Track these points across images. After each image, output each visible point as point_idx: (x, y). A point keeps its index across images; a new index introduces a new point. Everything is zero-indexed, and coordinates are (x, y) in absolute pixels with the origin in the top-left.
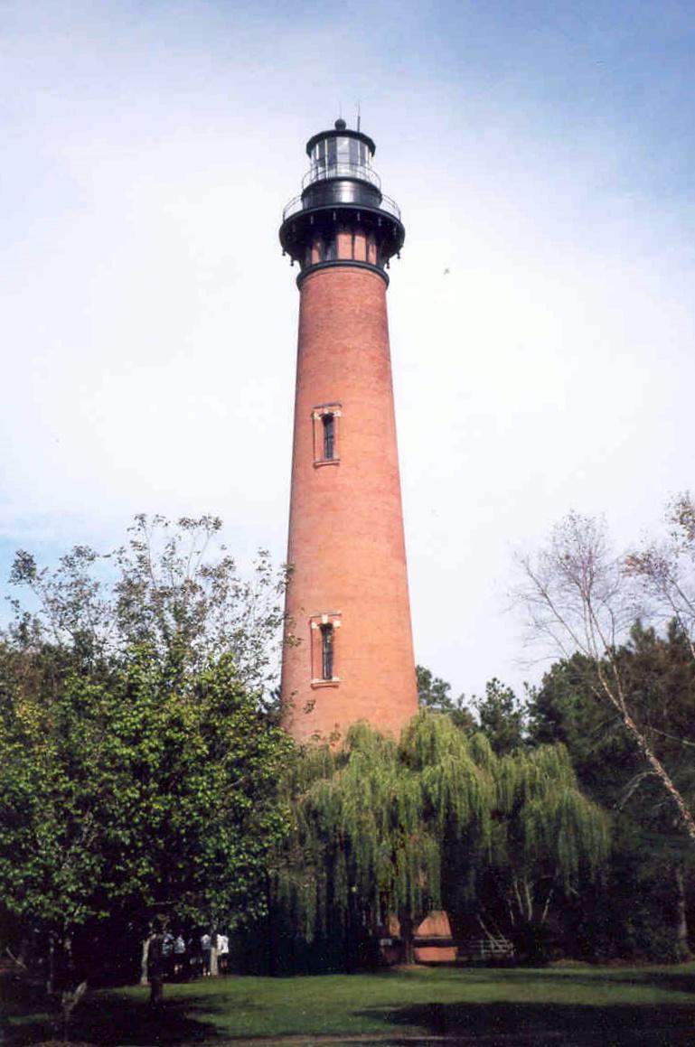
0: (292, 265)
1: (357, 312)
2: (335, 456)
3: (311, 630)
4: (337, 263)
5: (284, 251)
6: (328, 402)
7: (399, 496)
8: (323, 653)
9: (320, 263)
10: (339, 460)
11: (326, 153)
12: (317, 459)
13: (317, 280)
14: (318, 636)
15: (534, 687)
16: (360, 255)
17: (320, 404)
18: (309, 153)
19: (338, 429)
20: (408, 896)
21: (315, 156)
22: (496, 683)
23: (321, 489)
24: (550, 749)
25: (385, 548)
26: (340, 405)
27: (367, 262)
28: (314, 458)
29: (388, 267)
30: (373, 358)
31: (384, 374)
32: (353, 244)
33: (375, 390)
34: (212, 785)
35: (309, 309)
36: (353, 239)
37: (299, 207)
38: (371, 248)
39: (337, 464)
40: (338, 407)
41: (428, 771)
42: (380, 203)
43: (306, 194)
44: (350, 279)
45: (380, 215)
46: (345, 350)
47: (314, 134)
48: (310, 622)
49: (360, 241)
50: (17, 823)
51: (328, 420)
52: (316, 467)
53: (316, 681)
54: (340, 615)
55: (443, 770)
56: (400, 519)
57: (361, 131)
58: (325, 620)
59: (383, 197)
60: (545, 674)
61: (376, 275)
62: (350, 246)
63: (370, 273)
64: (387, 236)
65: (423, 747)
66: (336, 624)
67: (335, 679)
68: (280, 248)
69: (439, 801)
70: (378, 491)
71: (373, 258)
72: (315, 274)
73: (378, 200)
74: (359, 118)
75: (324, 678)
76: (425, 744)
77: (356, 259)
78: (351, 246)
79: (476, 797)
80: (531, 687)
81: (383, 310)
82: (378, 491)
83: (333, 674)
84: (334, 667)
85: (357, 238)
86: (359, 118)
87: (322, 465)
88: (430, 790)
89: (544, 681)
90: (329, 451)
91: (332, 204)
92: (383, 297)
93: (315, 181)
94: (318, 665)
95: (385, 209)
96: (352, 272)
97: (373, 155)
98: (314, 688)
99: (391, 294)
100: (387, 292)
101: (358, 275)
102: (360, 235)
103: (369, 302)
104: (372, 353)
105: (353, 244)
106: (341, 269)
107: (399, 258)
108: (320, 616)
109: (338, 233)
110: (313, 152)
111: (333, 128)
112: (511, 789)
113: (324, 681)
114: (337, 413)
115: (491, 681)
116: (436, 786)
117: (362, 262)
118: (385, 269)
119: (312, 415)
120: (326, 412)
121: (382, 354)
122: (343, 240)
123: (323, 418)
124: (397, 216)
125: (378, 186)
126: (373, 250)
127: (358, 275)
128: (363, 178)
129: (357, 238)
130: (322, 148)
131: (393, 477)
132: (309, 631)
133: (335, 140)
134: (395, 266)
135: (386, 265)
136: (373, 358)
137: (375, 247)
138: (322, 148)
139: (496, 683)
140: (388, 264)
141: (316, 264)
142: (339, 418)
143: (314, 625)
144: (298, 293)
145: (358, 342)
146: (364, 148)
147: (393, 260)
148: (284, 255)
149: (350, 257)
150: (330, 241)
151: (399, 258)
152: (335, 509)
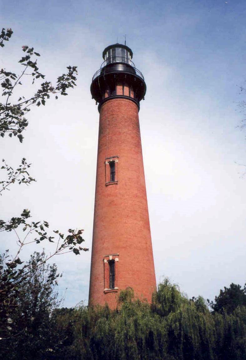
1: (126, 117)
2: (116, 180)
3: (104, 263)
4: (116, 97)
6: (112, 156)
7: (146, 200)
8: (110, 276)
9: (108, 97)
10: (117, 182)
11: (111, 54)
12: (107, 182)
13: (106, 105)
14: (108, 266)
15: (212, 302)
17: (109, 157)
19: (117, 169)
22: (194, 299)
23: (109, 195)
25: (141, 223)
26: (118, 157)
27: (129, 97)
28: (106, 182)
32: (123, 90)
33: (134, 151)
36: (123, 88)
38: (131, 92)
39: (117, 184)
40: (117, 158)
41: (171, 316)
43: (103, 70)
45: (135, 77)
46: (120, 133)
47: (106, 47)
48: (104, 260)
49: (126, 89)
51: (112, 164)
52: (107, 186)
53: (106, 289)
54: (118, 255)
55: (181, 313)
56: (149, 219)
57: (126, 45)
58: (111, 258)
60: (216, 297)
61: (134, 103)
62: (122, 91)
64: (139, 89)
65: (167, 302)
66: (117, 259)
67: (116, 288)
69: (179, 335)
70: (136, 196)
74: (125, 41)
75: (110, 288)
76: (168, 299)
78: (122, 90)
79: (204, 331)
80: (210, 302)
81: (137, 118)
82: (136, 196)
83: (115, 285)
84: (115, 282)
85: (125, 87)
86: (125, 41)
87: (109, 185)
88: (173, 326)
89: (216, 300)
90: (113, 178)
91: (115, 71)
92: (138, 114)
94: (107, 284)
98: (105, 293)
102: (125, 86)
103: (130, 113)
104: (132, 135)
105: (123, 90)
106: (118, 99)
108: (109, 256)
110: (105, 56)
112: (222, 332)
113: (110, 289)
114: (117, 161)
115: (192, 299)
116: (177, 324)
117: (128, 97)
119: (105, 163)
120: (111, 160)
121: (137, 136)
123: (109, 262)
126: (132, 93)
129: (125, 87)
130: (109, 53)
131: (143, 191)
132: (102, 265)
137: (133, 92)
138: (109, 53)
139: (194, 299)
141: (107, 98)
142: (117, 163)
143: (106, 261)
144: (98, 115)
145: (126, 131)
146: (128, 53)
149: (122, 94)
151: (144, 99)
152: (115, 205)
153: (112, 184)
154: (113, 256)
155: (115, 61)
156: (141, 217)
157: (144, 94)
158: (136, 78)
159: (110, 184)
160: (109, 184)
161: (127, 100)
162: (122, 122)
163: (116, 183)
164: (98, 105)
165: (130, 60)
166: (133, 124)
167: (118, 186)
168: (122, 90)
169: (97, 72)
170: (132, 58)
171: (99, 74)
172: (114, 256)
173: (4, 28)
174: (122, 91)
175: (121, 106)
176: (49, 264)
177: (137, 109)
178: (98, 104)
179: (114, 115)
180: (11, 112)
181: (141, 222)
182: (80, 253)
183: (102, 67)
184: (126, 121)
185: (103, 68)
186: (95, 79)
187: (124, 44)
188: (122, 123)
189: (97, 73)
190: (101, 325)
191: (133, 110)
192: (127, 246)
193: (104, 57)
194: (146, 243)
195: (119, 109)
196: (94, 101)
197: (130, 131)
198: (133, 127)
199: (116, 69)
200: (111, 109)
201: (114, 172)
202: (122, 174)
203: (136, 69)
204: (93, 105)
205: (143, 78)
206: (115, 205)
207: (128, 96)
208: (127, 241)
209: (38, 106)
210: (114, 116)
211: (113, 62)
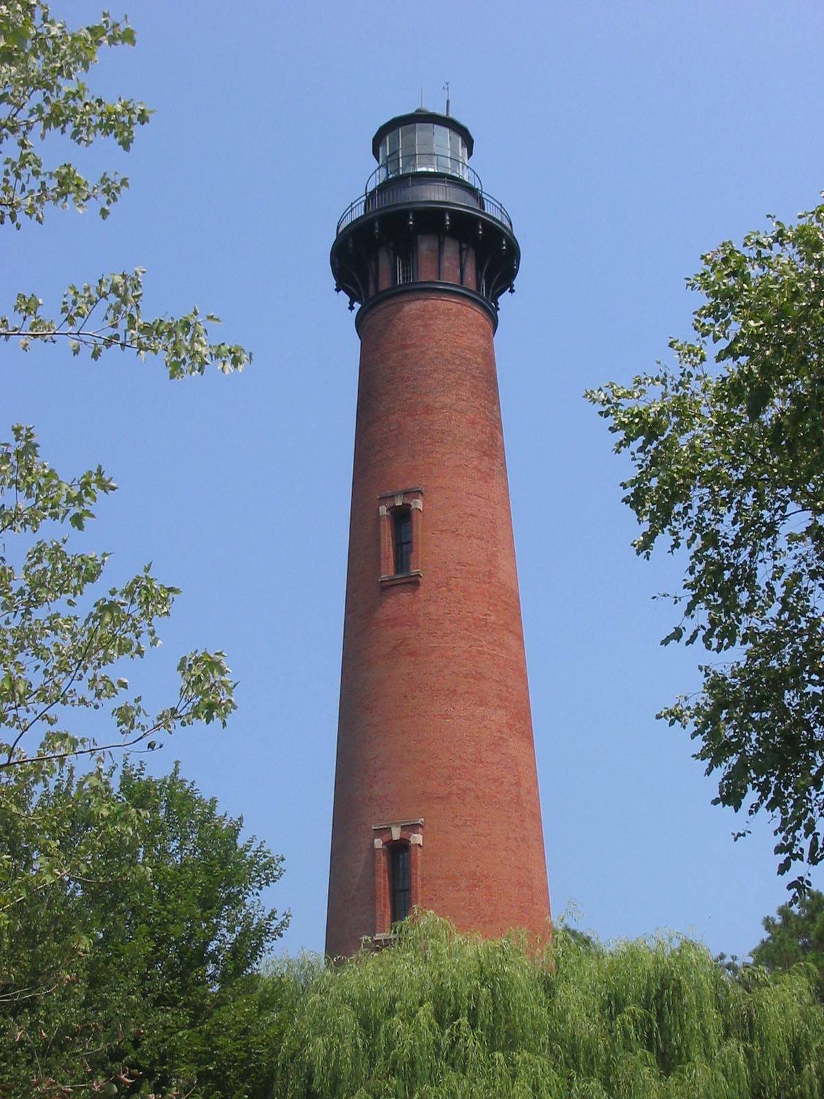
6: (401, 487)
14: (383, 862)
17: (389, 492)
19: (420, 531)
20: (70, 783)
31: (492, 448)
34: (715, 457)
43: (370, 197)
46: (428, 410)
50: (119, 1058)
51: (402, 517)
57: (451, 116)
58: (396, 834)
64: (492, 256)
66: (417, 838)
68: (333, 282)
72: (382, 306)
74: (448, 102)
86: (448, 102)
90: (402, 562)
92: (490, 341)
99: (500, 341)
125: (477, 186)
133: (414, 131)
138: (395, 142)
144: (357, 342)
150: (406, 252)
151: (512, 291)
152: (413, 654)
154: (402, 827)
155: (414, 166)
157: (512, 274)
158: (485, 223)
160: (388, 584)
162: (435, 370)
163: (414, 579)
164: (355, 312)
165: (464, 164)
167: (422, 593)
169: (352, 204)
170: (470, 154)
171: (359, 212)
172: (379, 832)
173: (175, 760)
175: (431, 319)
176: (601, 413)
177: (489, 326)
178: (357, 306)
182: (701, 679)
183: (369, 191)
184: (450, 367)
185: (373, 193)
186: (345, 229)
187: (445, 114)
188: (435, 375)
189: (351, 208)
190: (55, 672)
192: (450, 793)
193: (376, 153)
195: (425, 326)
196: (344, 298)
201: (409, 542)
202: (434, 549)
203: (484, 195)
204: (340, 312)
205: (511, 224)
206: (413, 654)
208: (450, 778)
209: (148, 122)
211: (406, 172)
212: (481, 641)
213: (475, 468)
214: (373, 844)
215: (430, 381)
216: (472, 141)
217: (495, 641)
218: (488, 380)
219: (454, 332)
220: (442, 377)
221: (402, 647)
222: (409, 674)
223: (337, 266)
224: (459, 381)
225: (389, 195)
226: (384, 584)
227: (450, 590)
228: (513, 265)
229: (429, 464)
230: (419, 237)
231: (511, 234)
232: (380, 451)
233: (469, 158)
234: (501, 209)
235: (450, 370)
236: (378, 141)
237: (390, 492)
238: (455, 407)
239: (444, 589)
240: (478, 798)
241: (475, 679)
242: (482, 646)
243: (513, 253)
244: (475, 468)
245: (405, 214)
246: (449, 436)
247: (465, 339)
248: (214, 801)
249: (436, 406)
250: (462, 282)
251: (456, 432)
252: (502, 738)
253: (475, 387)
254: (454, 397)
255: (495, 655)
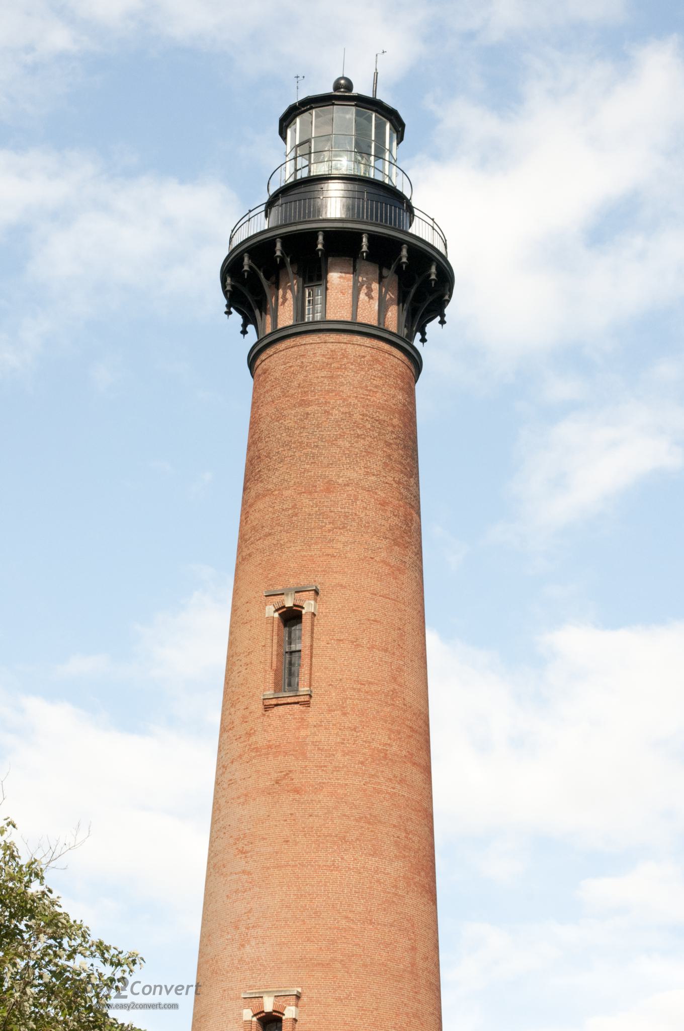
0: (244, 332)
1: (357, 417)
2: (303, 689)
5: (228, 306)
6: (293, 582)
13: (277, 359)
16: (368, 313)
17: (279, 588)
18: (283, 134)
21: (294, 138)
24: (330, 194)
29: (423, 340)
30: (384, 504)
35: (267, 410)
37: (260, 224)
39: (307, 704)
42: (410, 225)
44: (344, 356)
51: (291, 617)
58: (268, 1005)
59: (416, 212)
63: (387, 347)
68: (222, 301)
71: (393, 319)
73: (406, 216)
74: (376, 74)
77: (360, 319)
81: (408, 416)
86: (376, 74)
92: (411, 393)
93: (291, 180)
95: (414, 233)
96: (263, 361)
97: (400, 139)
100: (418, 386)
101: (361, 351)
103: (379, 398)
107: (442, 322)
109: (327, 274)
110: (289, 132)
111: (329, 89)
114: (309, 607)
118: (417, 343)
120: (289, 603)
122: (338, 280)
124: (441, 249)
127: (361, 351)
128: (379, 177)
134: (436, 342)
135: (418, 336)
136: (384, 504)
140: (423, 334)
147: (433, 327)
148: (228, 313)
151: (442, 322)
153: (288, 704)
156: (396, 844)
159: (247, 218)
160: (274, 702)
161: (367, 341)
163: (302, 699)
166: (389, 445)
167: (313, 715)
168: (344, 293)
174: (348, 298)
179: (308, 403)
180: (383, 182)
181: (399, 864)
184: (359, 432)
188: (340, 442)
191: (391, 381)
192: (334, 960)
194: (414, 949)
197: (373, 478)
198: (389, 456)
199: (319, 212)
200: (301, 377)
204: (233, 337)
205: (445, 245)
207: (375, 323)
210: (309, 410)
212: (378, 777)
213: (384, 562)
214: (240, 1015)
215: (334, 450)
216: (402, 125)
217: (395, 776)
218: (405, 446)
219: (367, 386)
220: (347, 445)
221: (284, 781)
222: (291, 814)
223: (228, 288)
224: (370, 450)
225: (295, 217)
226: (268, 702)
227: (345, 714)
228: (443, 296)
229: (328, 555)
230: (330, 259)
231: (445, 258)
232: (270, 534)
233: (398, 144)
234: (434, 226)
235: (358, 436)
236: (286, 121)
237: (280, 588)
238: (363, 483)
239: (338, 712)
240: (365, 965)
241: (369, 823)
242: (379, 783)
243: (446, 278)
244: (384, 562)
245: (313, 234)
246: (354, 520)
247: (378, 395)
248: (228, 313)
249: (340, 481)
250: (379, 323)
251: (362, 515)
252: (396, 894)
253: (389, 456)
254: (362, 472)
255: (395, 793)
